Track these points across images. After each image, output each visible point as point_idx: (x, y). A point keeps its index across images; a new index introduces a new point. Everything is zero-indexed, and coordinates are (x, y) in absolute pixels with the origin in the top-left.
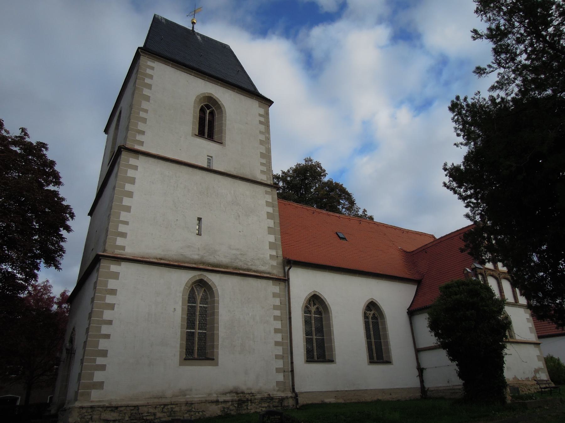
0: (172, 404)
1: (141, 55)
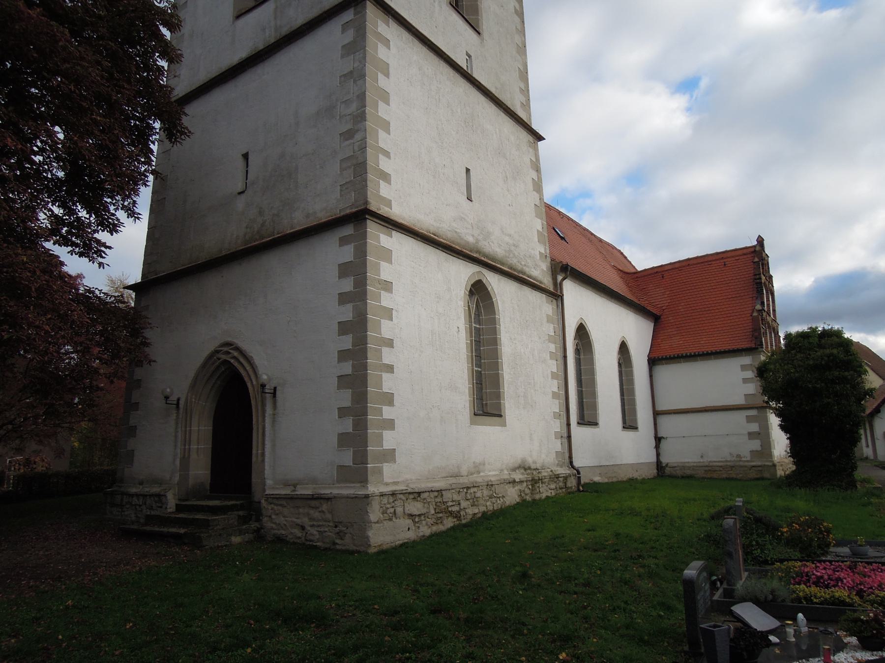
0: (474, 487)
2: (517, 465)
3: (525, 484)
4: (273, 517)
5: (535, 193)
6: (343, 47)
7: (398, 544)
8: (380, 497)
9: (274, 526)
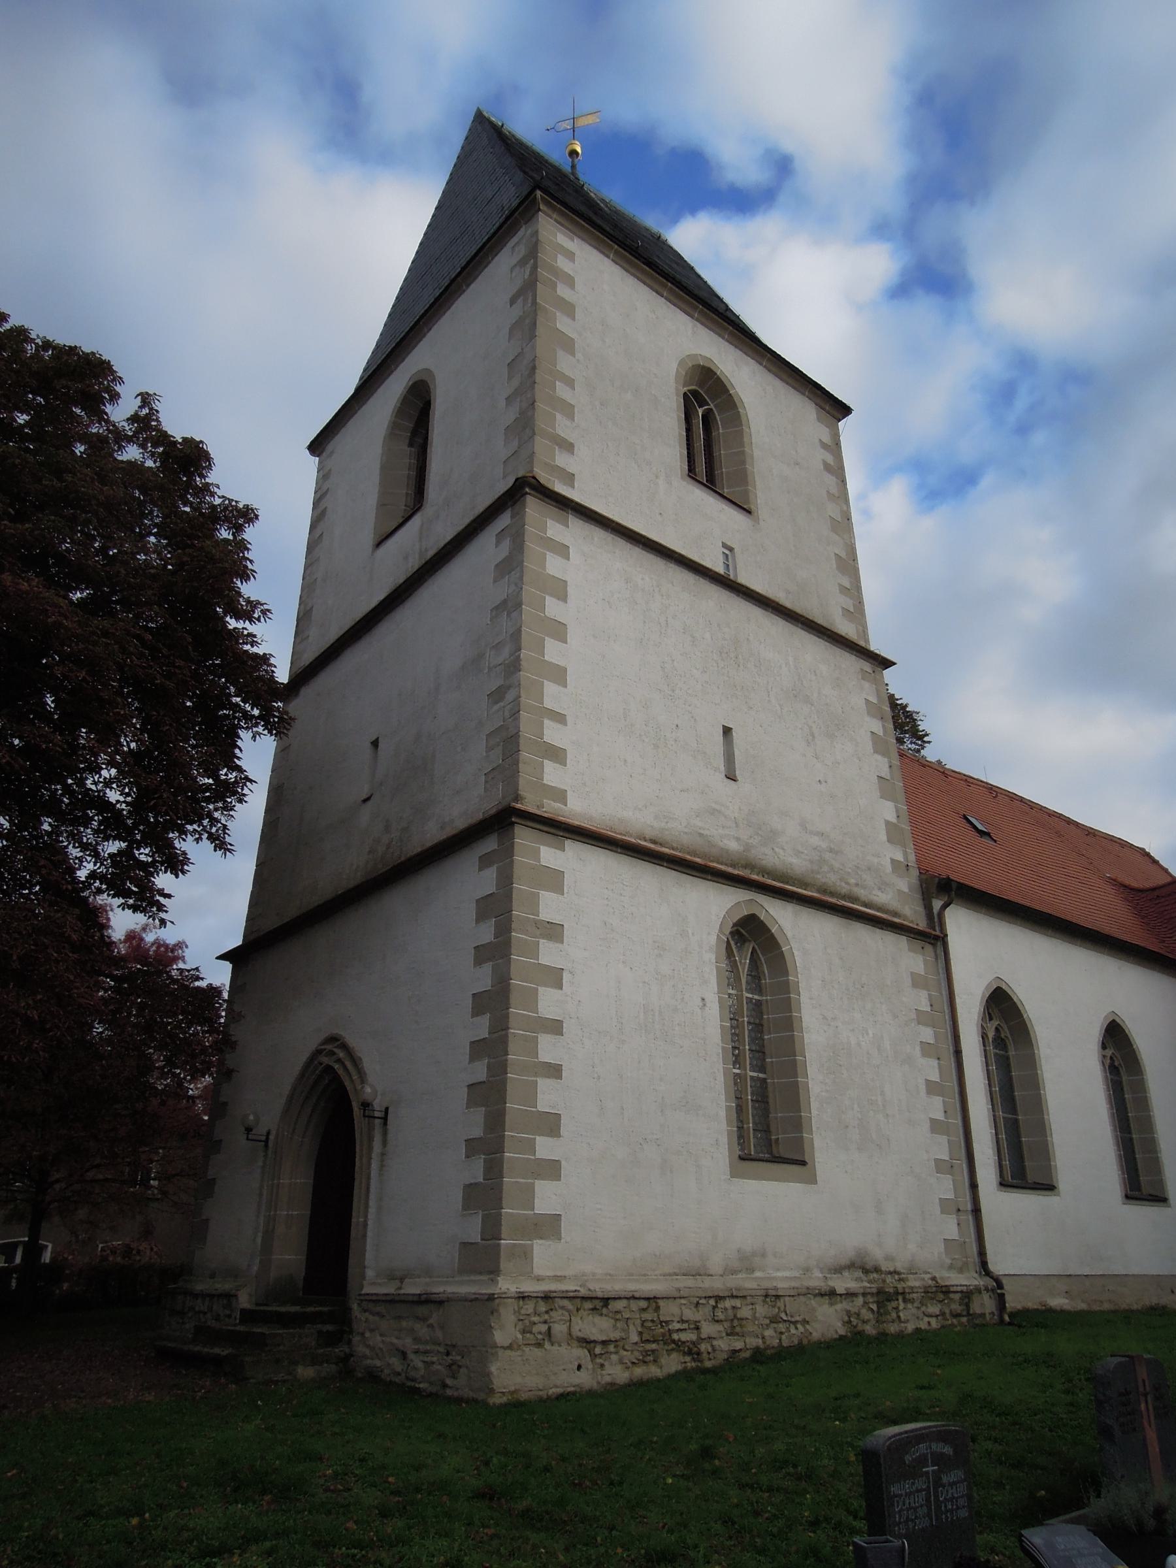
0: (733, 1297)
1: (539, 210)
2: (844, 1261)
3: (860, 1300)
4: (367, 1335)
5: (879, 757)
6: (497, 566)
7: (554, 1393)
8: (519, 1301)
9: (368, 1352)
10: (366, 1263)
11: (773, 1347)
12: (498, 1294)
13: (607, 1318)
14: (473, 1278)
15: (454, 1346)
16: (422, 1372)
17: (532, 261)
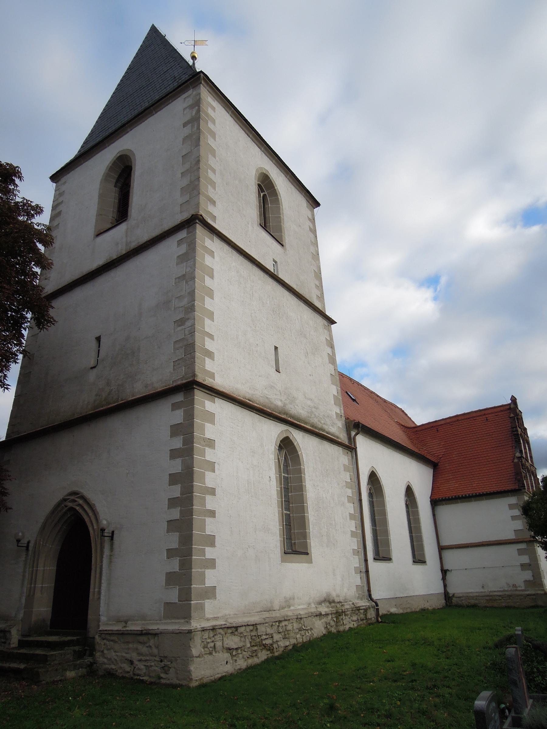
0: (285, 620)
2: (322, 599)
4: (105, 652)
6: (178, 257)
8: (202, 632)
9: (105, 661)
10: (100, 613)
11: (300, 643)
12: (194, 629)
13: (237, 636)
14: (173, 621)
15: (166, 657)
16: (144, 671)
17: (197, 107)
